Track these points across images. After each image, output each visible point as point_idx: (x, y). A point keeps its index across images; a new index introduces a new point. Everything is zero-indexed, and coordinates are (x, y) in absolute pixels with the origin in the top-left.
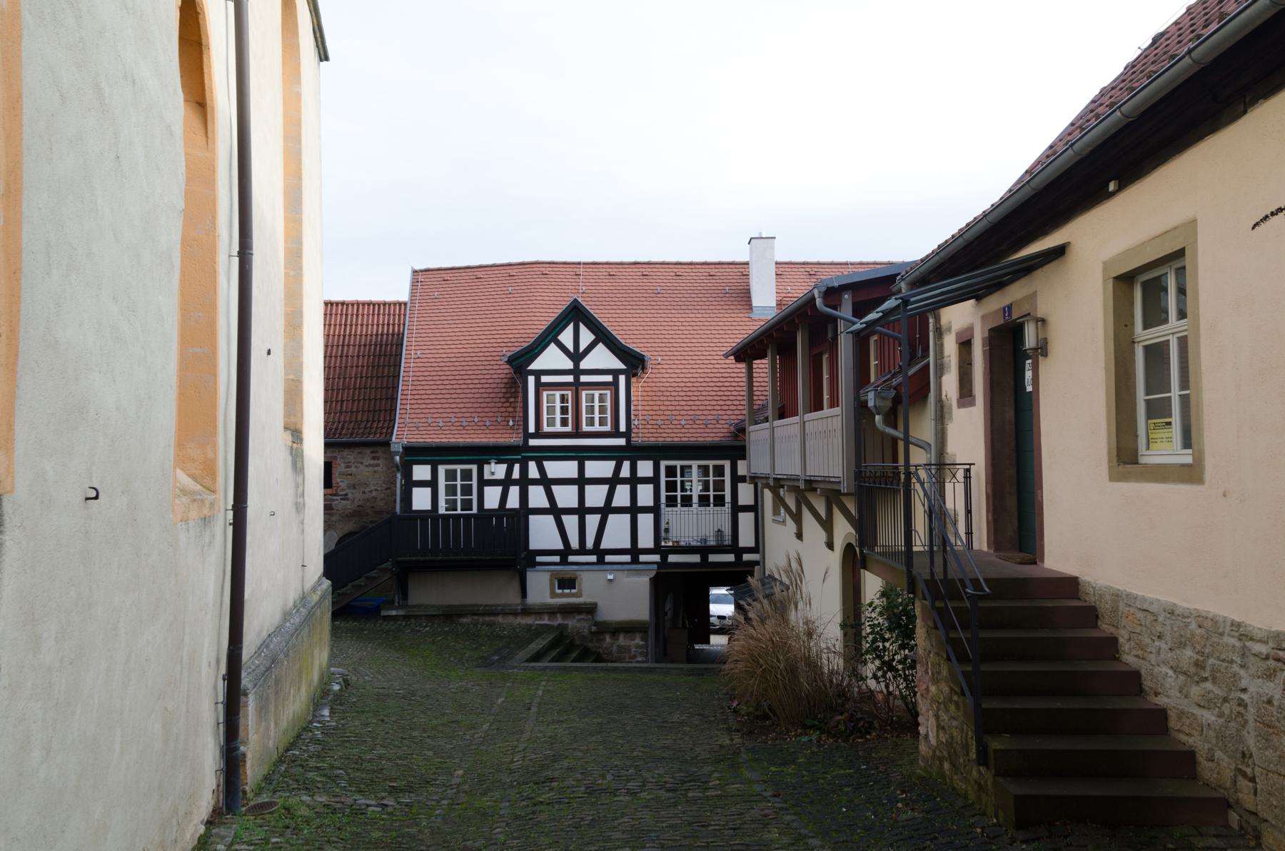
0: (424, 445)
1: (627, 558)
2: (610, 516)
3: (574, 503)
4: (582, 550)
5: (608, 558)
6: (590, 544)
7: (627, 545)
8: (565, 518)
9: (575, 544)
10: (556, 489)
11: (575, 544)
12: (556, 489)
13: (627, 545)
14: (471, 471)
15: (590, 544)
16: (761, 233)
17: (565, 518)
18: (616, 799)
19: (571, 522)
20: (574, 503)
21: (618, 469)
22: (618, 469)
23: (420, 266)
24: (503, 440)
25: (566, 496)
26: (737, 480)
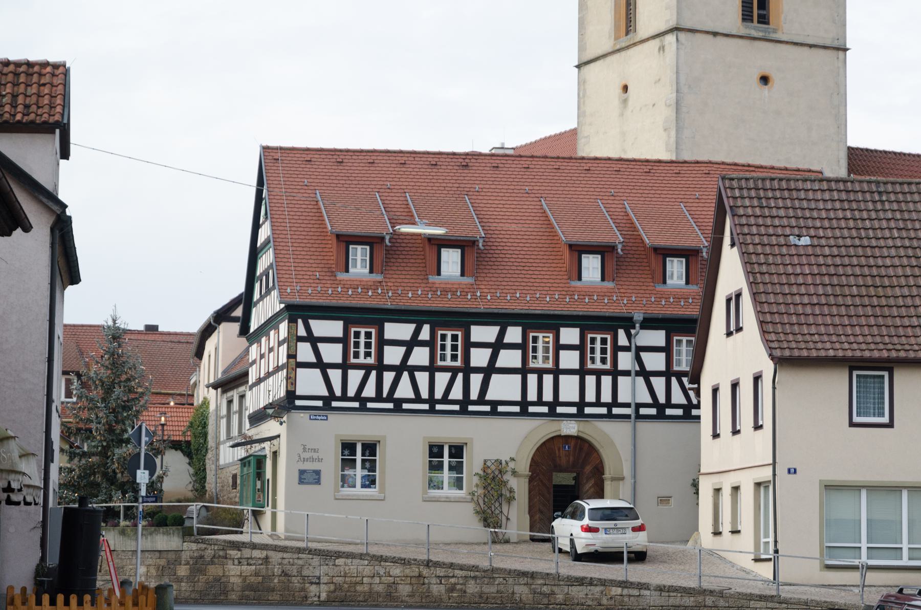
0: (671, 316)
1: (517, 409)
2: (493, 375)
3: (339, 359)
4: (344, 397)
5: (501, 409)
6: (351, 392)
7: (518, 398)
8: (330, 372)
9: (338, 392)
10: (321, 346)
11: (338, 392)
12: (321, 346)
13: (518, 398)
14: (676, 340)
15: (351, 392)
16: (503, 144)
17: (330, 372)
18: (281, 593)
19: (335, 376)
20: (339, 359)
21: (417, 332)
22: (417, 332)
23: (264, 144)
24: (309, 300)
25: (654, 361)
26: (617, 349)
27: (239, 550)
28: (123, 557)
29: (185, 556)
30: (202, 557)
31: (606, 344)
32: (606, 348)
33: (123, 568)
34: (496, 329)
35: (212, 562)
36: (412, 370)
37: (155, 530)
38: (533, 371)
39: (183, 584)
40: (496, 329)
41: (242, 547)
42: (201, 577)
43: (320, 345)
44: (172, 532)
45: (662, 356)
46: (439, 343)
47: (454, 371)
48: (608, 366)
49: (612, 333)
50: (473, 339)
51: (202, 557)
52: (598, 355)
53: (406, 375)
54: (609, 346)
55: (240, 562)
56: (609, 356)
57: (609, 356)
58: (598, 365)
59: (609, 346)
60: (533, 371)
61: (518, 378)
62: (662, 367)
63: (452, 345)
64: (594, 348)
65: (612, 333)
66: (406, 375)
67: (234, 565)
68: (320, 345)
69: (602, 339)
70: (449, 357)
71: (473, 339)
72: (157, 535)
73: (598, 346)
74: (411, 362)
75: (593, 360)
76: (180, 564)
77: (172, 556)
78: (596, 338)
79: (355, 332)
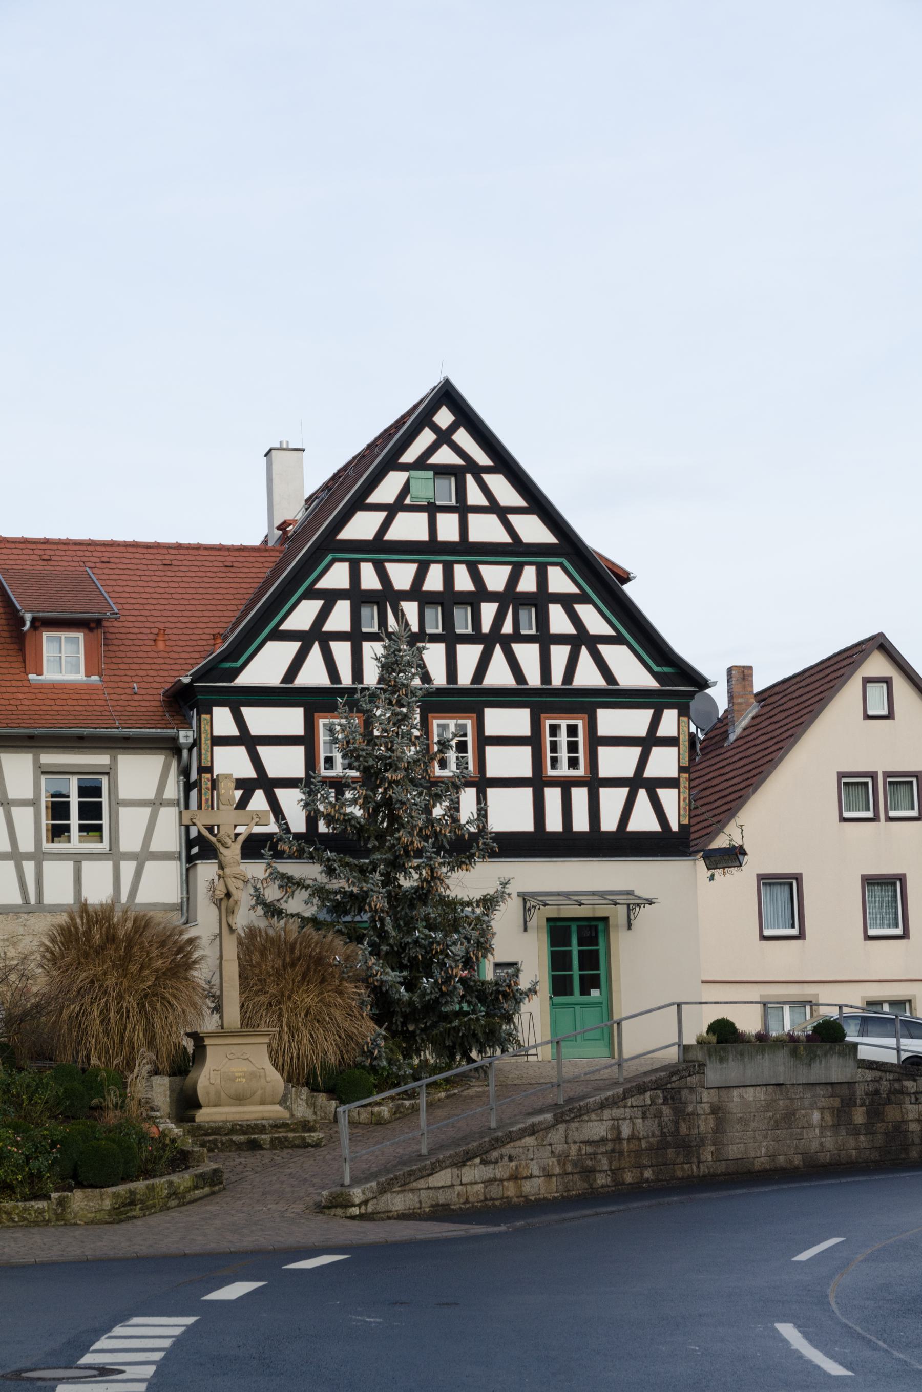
27: (915, 1080)
28: (793, 1097)
29: (860, 1090)
30: (877, 1092)
31: (576, 735)
32: (576, 742)
33: (794, 1115)
34: (648, 714)
35: (889, 1102)
36: (653, 785)
37: (831, 1048)
38: (554, 782)
39: (862, 1138)
40: (648, 714)
41: (917, 1075)
42: (879, 1125)
43: (261, 749)
44: (848, 1051)
45: (299, 752)
46: (548, 739)
47: (566, 785)
48: (581, 772)
49: (474, 715)
50: (602, 731)
51: (877, 1092)
52: (564, 754)
53: (642, 794)
54: (581, 739)
55: (917, 1099)
56: (581, 755)
57: (581, 755)
58: (564, 771)
59: (581, 739)
60: (554, 782)
61: (527, 793)
62: (299, 772)
63: (569, 743)
64: (556, 741)
65: (474, 715)
66: (642, 794)
67: (911, 1103)
68: (261, 749)
69: (568, 726)
70: (565, 762)
71: (602, 731)
72: (832, 1056)
73: (563, 739)
74: (650, 772)
75: (555, 762)
76: (855, 1106)
77: (845, 1091)
78: (559, 726)
79: (551, 726)
